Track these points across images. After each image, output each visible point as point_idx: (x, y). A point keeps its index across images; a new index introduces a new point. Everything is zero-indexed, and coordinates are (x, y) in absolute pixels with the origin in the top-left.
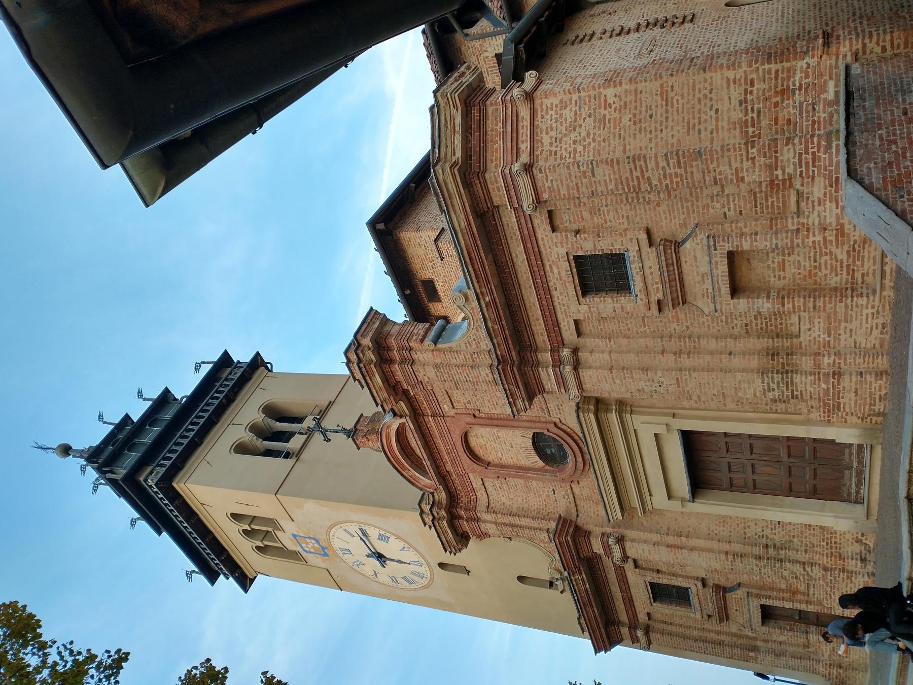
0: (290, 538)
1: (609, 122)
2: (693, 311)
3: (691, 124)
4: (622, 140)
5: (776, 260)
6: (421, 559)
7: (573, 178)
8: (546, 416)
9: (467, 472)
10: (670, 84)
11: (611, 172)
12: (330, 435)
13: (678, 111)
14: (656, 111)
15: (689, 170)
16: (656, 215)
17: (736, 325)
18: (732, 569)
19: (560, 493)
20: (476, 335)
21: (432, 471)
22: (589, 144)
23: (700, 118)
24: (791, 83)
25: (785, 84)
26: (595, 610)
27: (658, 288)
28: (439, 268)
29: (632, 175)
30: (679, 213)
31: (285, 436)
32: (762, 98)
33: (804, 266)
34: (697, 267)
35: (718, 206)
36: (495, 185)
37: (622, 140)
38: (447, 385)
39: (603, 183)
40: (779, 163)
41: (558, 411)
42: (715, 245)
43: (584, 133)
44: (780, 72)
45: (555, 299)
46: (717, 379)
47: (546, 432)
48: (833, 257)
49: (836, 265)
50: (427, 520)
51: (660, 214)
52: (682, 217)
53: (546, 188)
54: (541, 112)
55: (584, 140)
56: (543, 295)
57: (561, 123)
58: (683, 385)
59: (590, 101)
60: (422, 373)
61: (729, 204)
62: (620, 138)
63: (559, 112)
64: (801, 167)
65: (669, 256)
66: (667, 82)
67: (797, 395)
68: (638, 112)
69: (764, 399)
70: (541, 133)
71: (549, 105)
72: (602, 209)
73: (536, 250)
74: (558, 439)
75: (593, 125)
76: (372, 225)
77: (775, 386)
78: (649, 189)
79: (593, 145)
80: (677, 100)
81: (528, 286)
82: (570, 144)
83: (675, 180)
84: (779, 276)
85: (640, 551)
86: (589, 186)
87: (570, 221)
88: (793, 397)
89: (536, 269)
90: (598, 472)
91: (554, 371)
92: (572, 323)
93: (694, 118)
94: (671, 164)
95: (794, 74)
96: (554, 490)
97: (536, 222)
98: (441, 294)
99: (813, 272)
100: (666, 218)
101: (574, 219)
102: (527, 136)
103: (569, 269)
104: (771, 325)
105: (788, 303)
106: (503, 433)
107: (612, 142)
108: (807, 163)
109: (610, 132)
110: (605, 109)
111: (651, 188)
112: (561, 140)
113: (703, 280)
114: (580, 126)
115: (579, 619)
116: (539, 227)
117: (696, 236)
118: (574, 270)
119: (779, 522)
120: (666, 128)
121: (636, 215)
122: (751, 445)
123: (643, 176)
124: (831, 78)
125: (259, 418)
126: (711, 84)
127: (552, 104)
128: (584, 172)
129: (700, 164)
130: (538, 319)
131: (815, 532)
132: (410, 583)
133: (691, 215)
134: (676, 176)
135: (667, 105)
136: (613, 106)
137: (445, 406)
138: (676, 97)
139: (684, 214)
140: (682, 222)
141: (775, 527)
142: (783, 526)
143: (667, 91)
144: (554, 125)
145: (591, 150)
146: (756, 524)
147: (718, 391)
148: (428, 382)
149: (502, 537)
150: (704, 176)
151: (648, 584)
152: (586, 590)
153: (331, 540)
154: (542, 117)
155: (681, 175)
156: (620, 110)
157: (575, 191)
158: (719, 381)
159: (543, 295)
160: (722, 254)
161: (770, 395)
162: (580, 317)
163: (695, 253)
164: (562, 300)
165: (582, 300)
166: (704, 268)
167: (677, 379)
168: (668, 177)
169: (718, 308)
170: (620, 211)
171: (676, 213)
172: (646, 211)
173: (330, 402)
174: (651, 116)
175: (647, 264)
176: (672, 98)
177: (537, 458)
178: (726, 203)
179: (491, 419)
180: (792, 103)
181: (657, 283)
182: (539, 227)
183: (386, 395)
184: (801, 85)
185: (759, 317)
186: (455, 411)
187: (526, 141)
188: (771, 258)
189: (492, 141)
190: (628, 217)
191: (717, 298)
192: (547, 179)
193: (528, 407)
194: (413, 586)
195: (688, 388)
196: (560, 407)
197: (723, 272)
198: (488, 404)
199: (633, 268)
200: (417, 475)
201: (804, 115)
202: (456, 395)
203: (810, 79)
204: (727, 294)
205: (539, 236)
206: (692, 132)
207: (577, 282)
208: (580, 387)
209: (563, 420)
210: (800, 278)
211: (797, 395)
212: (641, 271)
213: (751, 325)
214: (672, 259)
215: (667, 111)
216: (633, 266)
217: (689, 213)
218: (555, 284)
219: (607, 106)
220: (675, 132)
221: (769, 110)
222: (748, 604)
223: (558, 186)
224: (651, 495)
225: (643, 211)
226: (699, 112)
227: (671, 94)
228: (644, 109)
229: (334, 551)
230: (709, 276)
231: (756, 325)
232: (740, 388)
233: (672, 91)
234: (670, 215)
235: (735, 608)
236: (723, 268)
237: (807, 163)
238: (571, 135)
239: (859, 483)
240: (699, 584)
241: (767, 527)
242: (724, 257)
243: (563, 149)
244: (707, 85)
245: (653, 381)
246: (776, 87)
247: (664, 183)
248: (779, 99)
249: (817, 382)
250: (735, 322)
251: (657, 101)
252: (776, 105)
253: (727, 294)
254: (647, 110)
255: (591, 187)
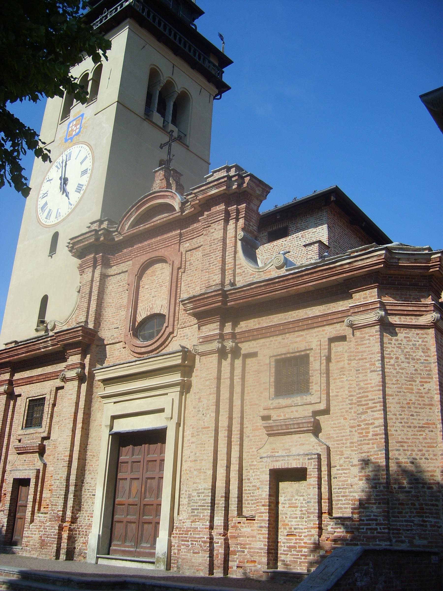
0: (80, 111)
1: (410, 385)
2: (261, 441)
3: (404, 444)
4: (396, 393)
5: (297, 501)
6: (62, 218)
7: (371, 356)
8: (179, 326)
9: (134, 260)
10: (434, 430)
11: (373, 385)
12: (166, 148)
13: (414, 435)
14: (416, 419)
15: (371, 442)
16: (337, 416)
17: (249, 472)
18: (58, 459)
19: (116, 333)
20: (248, 273)
21: (135, 231)
22: (396, 369)
23: (408, 450)
24: (427, 515)
25: (427, 511)
26: (24, 355)
27: (280, 416)
28: (297, 243)
29: (370, 400)
30: (337, 433)
31: (162, 111)
32: (419, 494)
33: (292, 521)
34: (296, 445)
35: (342, 462)
36: (368, 296)
37: (396, 393)
38: (207, 247)
39: (365, 378)
40: (371, 505)
41: (182, 335)
42: (312, 459)
43: (403, 365)
44: (437, 508)
45: (275, 338)
46: (208, 457)
47: (165, 325)
48: (298, 541)
49: (291, 543)
50: (95, 225)
51: (338, 419)
52: (335, 436)
53: (363, 335)
54: (422, 334)
55: (398, 366)
56: (279, 328)
57: (412, 349)
58: (203, 431)
59: (426, 370)
60: (217, 228)
61: (343, 469)
62: (397, 392)
63: (420, 347)
64: (367, 520)
65: (305, 425)
66: (436, 427)
67: (194, 512)
68: (416, 406)
69: (191, 490)
70: (405, 333)
71: (426, 340)
72: (344, 376)
73: (315, 325)
74: (160, 334)
75: (409, 372)
76: (336, 191)
77: (201, 498)
78: (358, 412)
79: (394, 372)
80: (422, 435)
81: (287, 317)
82: (396, 354)
83: (364, 431)
84: (285, 504)
85: (71, 392)
86: (363, 367)
87: (337, 352)
88: (193, 509)
89: (300, 324)
90: (134, 364)
91: (216, 335)
92: (255, 350)
93: (408, 446)
94: (376, 429)
95: (434, 517)
96: (118, 328)
97: (338, 326)
98: (275, 243)
99: (287, 527)
100: (334, 424)
101: (338, 355)
102: (404, 322)
103: (299, 350)
104: (248, 497)
105: (265, 509)
106: (165, 290)
107: (396, 386)
108: (369, 524)
109: (402, 384)
110: (420, 382)
111: (358, 414)
112: (399, 347)
113: (285, 450)
114: (409, 363)
115: (16, 342)
116: (333, 328)
117: (320, 446)
118: (298, 354)
119: (94, 495)
120: (403, 426)
121: (338, 402)
122: (154, 478)
123: (368, 408)
124: (429, 542)
125: (178, 88)
126: (431, 459)
127: (426, 342)
128: (374, 364)
129: (374, 450)
130: (259, 323)
131: (87, 520)
132: (42, 208)
133: (335, 443)
134: (366, 433)
135: (419, 427)
136: (422, 388)
137: (188, 244)
138: (424, 434)
139: (337, 437)
140: (331, 435)
141: (90, 492)
142: (91, 498)
143: (429, 427)
144: (411, 343)
145: (391, 370)
146: (92, 479)
147: (199, 457)
148: (209, 232)
149: (80, 285)
150: (365, 452)
151: (44, 396)
152: (39, 349)
153: (78, 146)
154: (418, 334)
155: (367, 436)
156: (418, 393)
157: (360, 357)
158: (206, 458)
159: (279, 328)
160: (305, 464)
161: (195, 494)
162: (260, 357)
163: (306, 444)
164: (274, 344)
165: (273, 359)
166: (295, 451)
167: (209, 427)
168: (367, 426)
169: (263, 459)
170: (342, 390)
171: (338, 431)
172: (341, 409)
173: (188, 147)
174: (412, 415)
175: (300, 408)
176: (424, 431)
177: (144, 316)
178: (343, 467)
179: (177, 282)
180: (413, 515)
181: (285, 416)
182: (333, 328)
183: (201, 197)
184: (426, 521)
185: (254, 488)
186: (184, 253)
187: (400, 321)
188: (299, 498)
189: (402, 294)
190: (337, 396)
191: (271, 459)
192: (371, 336)
193: (188, 312)
194: (39, 210)
195: (201, 435)
196: (186, 337)
197: (291, 464)
198: (189, 279)
199: (298, 399)
200: (132, 219)
201: (404, 523)
202: (198, 254)
203: (430, 528)
204: (274, 466)
205: (327, 328)
206: (398, 445)
207: (288, 355)
208: (202, 354)
209: (175, 338)
210: (283, 518)
211: (194, 512)
212: (295, 404)
213: (248, 483)
214: (302, 428)
215: (415, 427)
216: (299, 398)
217: (337, 441)
218: (287, 338)
219: (422, 383)
220: (399, 432)
221: (410, 499)
222: (30, 469)
223: (365, 344)
224: (115, 403)
225: (341, 407)
226: (413, 450)
227: (427, 431)
228: (418, 410)
229: (69, 147)
230: (288, 454)
231: (248, 486)
232: (200, 473)
233: (429, 431)
234: (336, 427)
235: (27, 459)
236: (294, 464)
237: (369, 524)
238: (402, 356)
239: (124, 553)
240: (45, 435)
241: (90, 486)
242: (303, 465)
243: (393, 349)
244: (431, 456)
245: (207, 409)
246: (427, 505)
247: (362, 424)
248: (417, 506)
249: (204, 526)
250: (251, 471)
251: (423, 420)
252: (413, 504)
253: (274, 466)
254: (417, 412)
255: (363, 370)
